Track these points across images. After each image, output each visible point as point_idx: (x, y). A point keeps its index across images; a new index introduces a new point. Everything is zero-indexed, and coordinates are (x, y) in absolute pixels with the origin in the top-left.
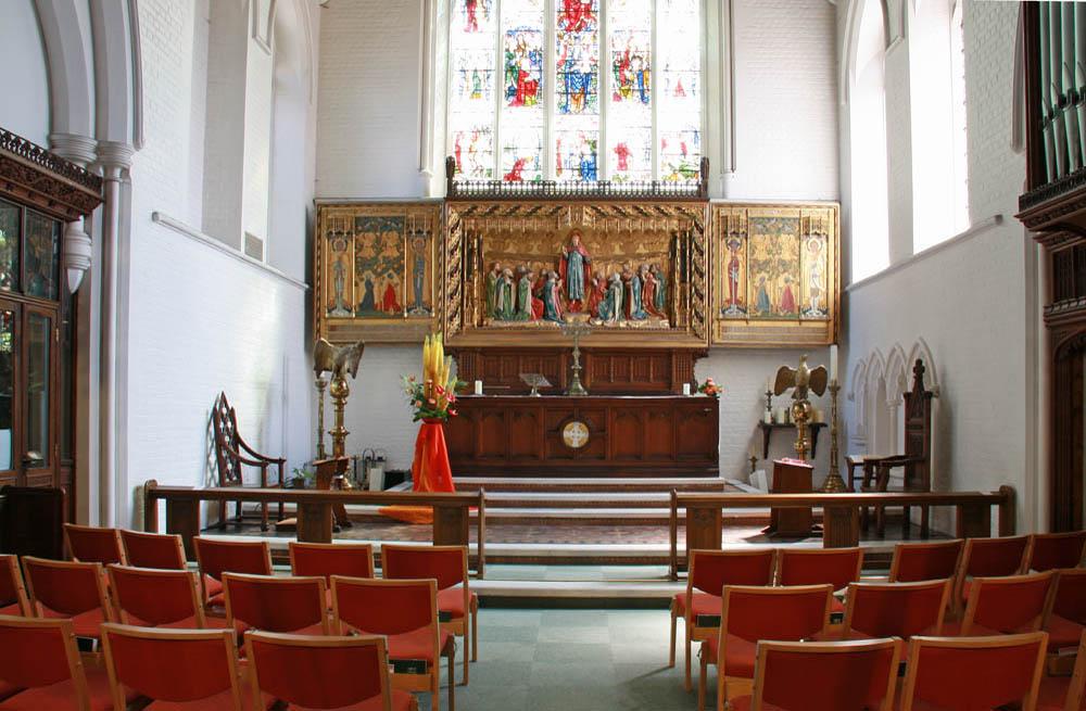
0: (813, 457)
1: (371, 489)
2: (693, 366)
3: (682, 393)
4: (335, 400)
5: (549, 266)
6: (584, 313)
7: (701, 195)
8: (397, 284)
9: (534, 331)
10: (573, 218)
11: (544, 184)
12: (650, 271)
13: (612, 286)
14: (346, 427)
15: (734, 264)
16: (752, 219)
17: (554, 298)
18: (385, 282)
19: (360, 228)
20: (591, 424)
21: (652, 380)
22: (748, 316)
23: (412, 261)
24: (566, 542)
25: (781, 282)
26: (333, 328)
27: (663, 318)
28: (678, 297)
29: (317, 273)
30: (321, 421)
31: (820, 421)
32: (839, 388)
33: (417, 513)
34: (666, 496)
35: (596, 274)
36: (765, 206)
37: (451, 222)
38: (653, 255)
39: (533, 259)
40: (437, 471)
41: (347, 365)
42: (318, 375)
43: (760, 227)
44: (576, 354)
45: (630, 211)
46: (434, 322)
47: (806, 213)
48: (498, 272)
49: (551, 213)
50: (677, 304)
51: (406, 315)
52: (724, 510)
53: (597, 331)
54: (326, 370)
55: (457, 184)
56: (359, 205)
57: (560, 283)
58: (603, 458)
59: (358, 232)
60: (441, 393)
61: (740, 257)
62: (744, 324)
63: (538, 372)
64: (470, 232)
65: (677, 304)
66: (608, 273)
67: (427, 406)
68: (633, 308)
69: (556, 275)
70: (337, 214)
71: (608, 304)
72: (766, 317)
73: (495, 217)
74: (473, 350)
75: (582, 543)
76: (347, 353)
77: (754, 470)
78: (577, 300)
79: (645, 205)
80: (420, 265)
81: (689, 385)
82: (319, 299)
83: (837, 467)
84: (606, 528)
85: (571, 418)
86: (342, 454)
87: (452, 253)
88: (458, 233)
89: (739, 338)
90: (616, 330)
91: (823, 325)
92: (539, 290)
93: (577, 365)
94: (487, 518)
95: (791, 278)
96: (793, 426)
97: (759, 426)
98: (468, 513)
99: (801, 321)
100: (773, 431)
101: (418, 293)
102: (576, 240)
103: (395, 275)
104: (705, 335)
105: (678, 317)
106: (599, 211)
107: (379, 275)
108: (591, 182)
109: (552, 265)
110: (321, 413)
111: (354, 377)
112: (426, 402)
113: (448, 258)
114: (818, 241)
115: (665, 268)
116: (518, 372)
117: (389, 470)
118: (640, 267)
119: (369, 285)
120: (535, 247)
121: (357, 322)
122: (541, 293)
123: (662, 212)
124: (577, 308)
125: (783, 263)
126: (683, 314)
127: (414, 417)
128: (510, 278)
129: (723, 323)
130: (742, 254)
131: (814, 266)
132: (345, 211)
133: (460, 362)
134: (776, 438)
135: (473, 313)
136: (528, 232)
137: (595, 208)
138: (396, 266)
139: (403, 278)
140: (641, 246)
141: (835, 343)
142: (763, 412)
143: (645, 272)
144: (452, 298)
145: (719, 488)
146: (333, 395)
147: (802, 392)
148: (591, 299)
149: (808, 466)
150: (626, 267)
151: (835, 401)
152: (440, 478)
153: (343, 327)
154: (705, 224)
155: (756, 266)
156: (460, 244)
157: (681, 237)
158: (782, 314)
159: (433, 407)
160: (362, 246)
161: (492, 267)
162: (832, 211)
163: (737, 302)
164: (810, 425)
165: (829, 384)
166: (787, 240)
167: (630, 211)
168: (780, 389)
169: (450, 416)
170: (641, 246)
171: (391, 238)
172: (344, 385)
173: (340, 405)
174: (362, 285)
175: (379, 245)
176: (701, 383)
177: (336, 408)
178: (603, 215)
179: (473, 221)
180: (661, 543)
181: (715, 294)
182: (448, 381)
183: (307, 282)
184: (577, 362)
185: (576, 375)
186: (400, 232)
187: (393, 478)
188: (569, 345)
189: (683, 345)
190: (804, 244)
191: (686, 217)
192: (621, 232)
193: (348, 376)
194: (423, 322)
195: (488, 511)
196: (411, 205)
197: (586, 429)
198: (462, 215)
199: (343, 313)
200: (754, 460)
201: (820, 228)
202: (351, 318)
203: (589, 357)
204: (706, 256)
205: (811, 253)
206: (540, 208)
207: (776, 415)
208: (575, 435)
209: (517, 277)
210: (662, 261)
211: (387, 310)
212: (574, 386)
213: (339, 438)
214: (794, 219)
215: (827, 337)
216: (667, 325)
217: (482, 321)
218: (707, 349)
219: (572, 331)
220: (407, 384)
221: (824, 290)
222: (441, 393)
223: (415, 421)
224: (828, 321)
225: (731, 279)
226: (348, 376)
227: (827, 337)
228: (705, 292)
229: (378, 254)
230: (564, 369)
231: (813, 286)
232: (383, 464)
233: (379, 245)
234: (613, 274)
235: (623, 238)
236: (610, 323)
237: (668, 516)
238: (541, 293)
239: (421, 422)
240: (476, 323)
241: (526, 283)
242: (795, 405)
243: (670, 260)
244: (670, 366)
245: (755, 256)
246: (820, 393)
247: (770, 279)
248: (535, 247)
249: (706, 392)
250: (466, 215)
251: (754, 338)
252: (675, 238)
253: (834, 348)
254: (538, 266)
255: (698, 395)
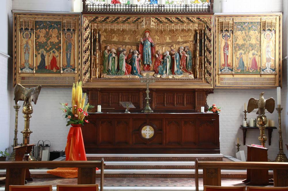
0: (270, 144)
1: (42, 160)
2: (206, 98)
3: (200, 112)
4: (25, 115)
5: (134, 48)
6: (152, 71)
7: (210, 11)
8: (57, 56)
9: (127, 80)
10: (146, 24)
11: (131, 6)
12: (184, 50)
13: (165, 58)
14: (31, 129)
15: (226, 46)
16: (236, 23)
17: (136, 64)
18: (51, 55)
19: (38, 27)
20: (155, 126)
21: (185, 105)
22: (233, 73)
23: (65, 44)
24: (144, 186)
25: (251, 55)
26: (23, 78)
27: (191, 74)
28: (198, 63)
29: (14, 50)
30: (17, 126)
31: (273, 125)
32: (282, 109)
33: (67, 172)
34: (193, 163)
35: (157, 51)
36: (242, 16)
37: (85, 25)
38: (186, 42)
39: (126, 44)
40: (79, 150)
41: (32, 97)
42: (16, 103)
43: (239, 27)
44: (148, 92)
45: (174, 20)
46: (77, 75)
47: (264, 19)
48: (109, 51)
49: (135, 21)
50: (198, 67)
51: (62, 72)
52: (222, 171)
53: (158, 80)
54: (21, 100)
55: (87, 6)
56: (37, 14)
57: (140, 57)
58: (161, 144)
59: (36, 29)
60: (81, 111)
61: (229, 43)
62: (232, 76)
63: (129, 101)
64: (95, 30)
65: (198, 67)
66: (164, 51)
67: (73, 118)
68: (176, 69)
69: (137, 52)
70: (26, 19)
71: (163, 67)
72: (243, 73)
73: (107, 23)
74: (96, 90)
75: (152, 186)
76: (32, 91)
77: (238, 151)
78: (148, 65)
79: (181, 17)
80: (69, 47)
81: (204, 107)
82: (16, 63)
83: (282, 150)
84: (163, 179)
85: (145, 124)
86: (28, 143)
87: (86, 41)
88: (89, 31)
89: (229, 84)
90: (168, 80)
91: (273, 76)
92: (129, 60)
93: (148, 97)
94: (105, 174)
95: (256, 53)
96: (258, 128)
97: (240, 128)
98: (95, 172)
99: (261, 75)
100: (248, 131)
101: (69, 61)
102: (147, 34)
103: (56, 52)
104: (212, 82)
105: (198, 73)
106: (158, 20)
107: (48, 51)
108: (155, 5)
109: (136, 47)
110: (16, 122)
111: (35, 103)
112: (73, 116)
113: (83, 43)
114: (270, 34)
115: (192, 49)
116: (119, 101)
117: (52, 151)
118: (179, 48)
119: (43, 57)
120: (127, 38)
121: (36, 75)
122: (130, 61)
123: (190, 20)
124: (148, 69)
125: (251, 45)
126: (201, 72)
127: (67, 123)
128: (115, 53)
129: (221, 76)
130: (230, 41)
131: (268, 47)
132: (29, 18)
133: (90, 96)
134: (250, 134)
135: (96, 71)
136: (123, 31)
137: (157, 19)
138: (57, 47)
139: (60, 53)
140: (180, 37)
141: (280, 86)
142: (242, 121)
143: (181, 51)
144: (85, 64)
145: (221, 159)
146: (25, 113)
147: (262, 111)
148: (155, 64)
149: (265, 148)
150: (172, 48)
151: (280, 116)
152: (80, 154)
153: (29, 77)
154: (212, 26)
155: (241, 47)
156: (90, 36)
157: (200, 33)
158: (251, 71)
159: (77, 118)
160: (39, 36)
161: (106, 48)
162: (278, 18)
163: (228, 65)
164: (267, 128)
165: (276, 107)
166: (254, 34)
167: (174, 20)
168: (250, 109)
169: (85, 123)
170: (180, 37)
171: (54, 33)
172: (30, 107)
173: (28, 118)
174: (39, 57)
175: (48, 36)
176: (210, 106)
177: (26, 120)
178: (161, 22)
179: (96, 25)
180: (191, 186)
181: (217, 61)
182: (84, 105)
183: (9, 54)
184: (148, 96)
185: (148, 102)
186: (59, 30)
187: (54, 155)
188: (144, 87)
189: (201, 87)
190: (262, 35)
191: (202, 22)
192: (170, 30)
193: (32, 103)
194: (70, 75)
195: (106, 171)
196: (64, 15)
197: (153, 129)
198: (91, 21)
199: (29, 71)
200: (238, 145)
201: (271, 27)
202: (33, 73)
203: (154, 93)
204: (212, 42)
205: (266, 40)
206: (129, 18)
207: (249, 123)
208: (147, 132)
209: (118, 53)
210: (190, 45)
211: (52, 69)
212: (147, 108)
213: (27, 134)
214: (258, 22)
215: (275, 83)
216: (193, 77)
217: (101, 75)
218: (213, 89)
219: (146, 80)
220: (64, 107)
221: (273, 58)
222: (81, 111)
223: (67, 125)
224: (276, 75)
225: (225, 54)
226: (32, 103)
227: (275, 83)
228: (212, 60)
229: (47, 40)
230: (141, 99)
231: (268, 57)
232: (48, 148)
233: (48, 36)
234: (166, 52)
235: (171, 33)
236: (164, 76)
237: (194, 173)
238: (130, 61)
239: (70, 126)
240: (97, 76)
241: (122, 56)
242: (258, 117)
243: (194, 44)
244: (194, 98)
245: (237, 42)
246: (271, 111)
247: (245, 53)
248: (127, 38)
249: (212, 111)
250: (93, 21)
251: (237, 83)
252: (196, 33)
253: (279, 89)
254: (129, 48)
255: (208, 112)
